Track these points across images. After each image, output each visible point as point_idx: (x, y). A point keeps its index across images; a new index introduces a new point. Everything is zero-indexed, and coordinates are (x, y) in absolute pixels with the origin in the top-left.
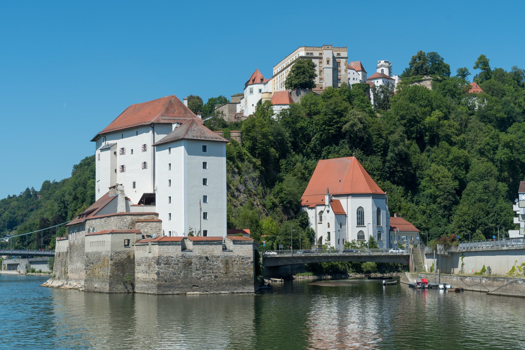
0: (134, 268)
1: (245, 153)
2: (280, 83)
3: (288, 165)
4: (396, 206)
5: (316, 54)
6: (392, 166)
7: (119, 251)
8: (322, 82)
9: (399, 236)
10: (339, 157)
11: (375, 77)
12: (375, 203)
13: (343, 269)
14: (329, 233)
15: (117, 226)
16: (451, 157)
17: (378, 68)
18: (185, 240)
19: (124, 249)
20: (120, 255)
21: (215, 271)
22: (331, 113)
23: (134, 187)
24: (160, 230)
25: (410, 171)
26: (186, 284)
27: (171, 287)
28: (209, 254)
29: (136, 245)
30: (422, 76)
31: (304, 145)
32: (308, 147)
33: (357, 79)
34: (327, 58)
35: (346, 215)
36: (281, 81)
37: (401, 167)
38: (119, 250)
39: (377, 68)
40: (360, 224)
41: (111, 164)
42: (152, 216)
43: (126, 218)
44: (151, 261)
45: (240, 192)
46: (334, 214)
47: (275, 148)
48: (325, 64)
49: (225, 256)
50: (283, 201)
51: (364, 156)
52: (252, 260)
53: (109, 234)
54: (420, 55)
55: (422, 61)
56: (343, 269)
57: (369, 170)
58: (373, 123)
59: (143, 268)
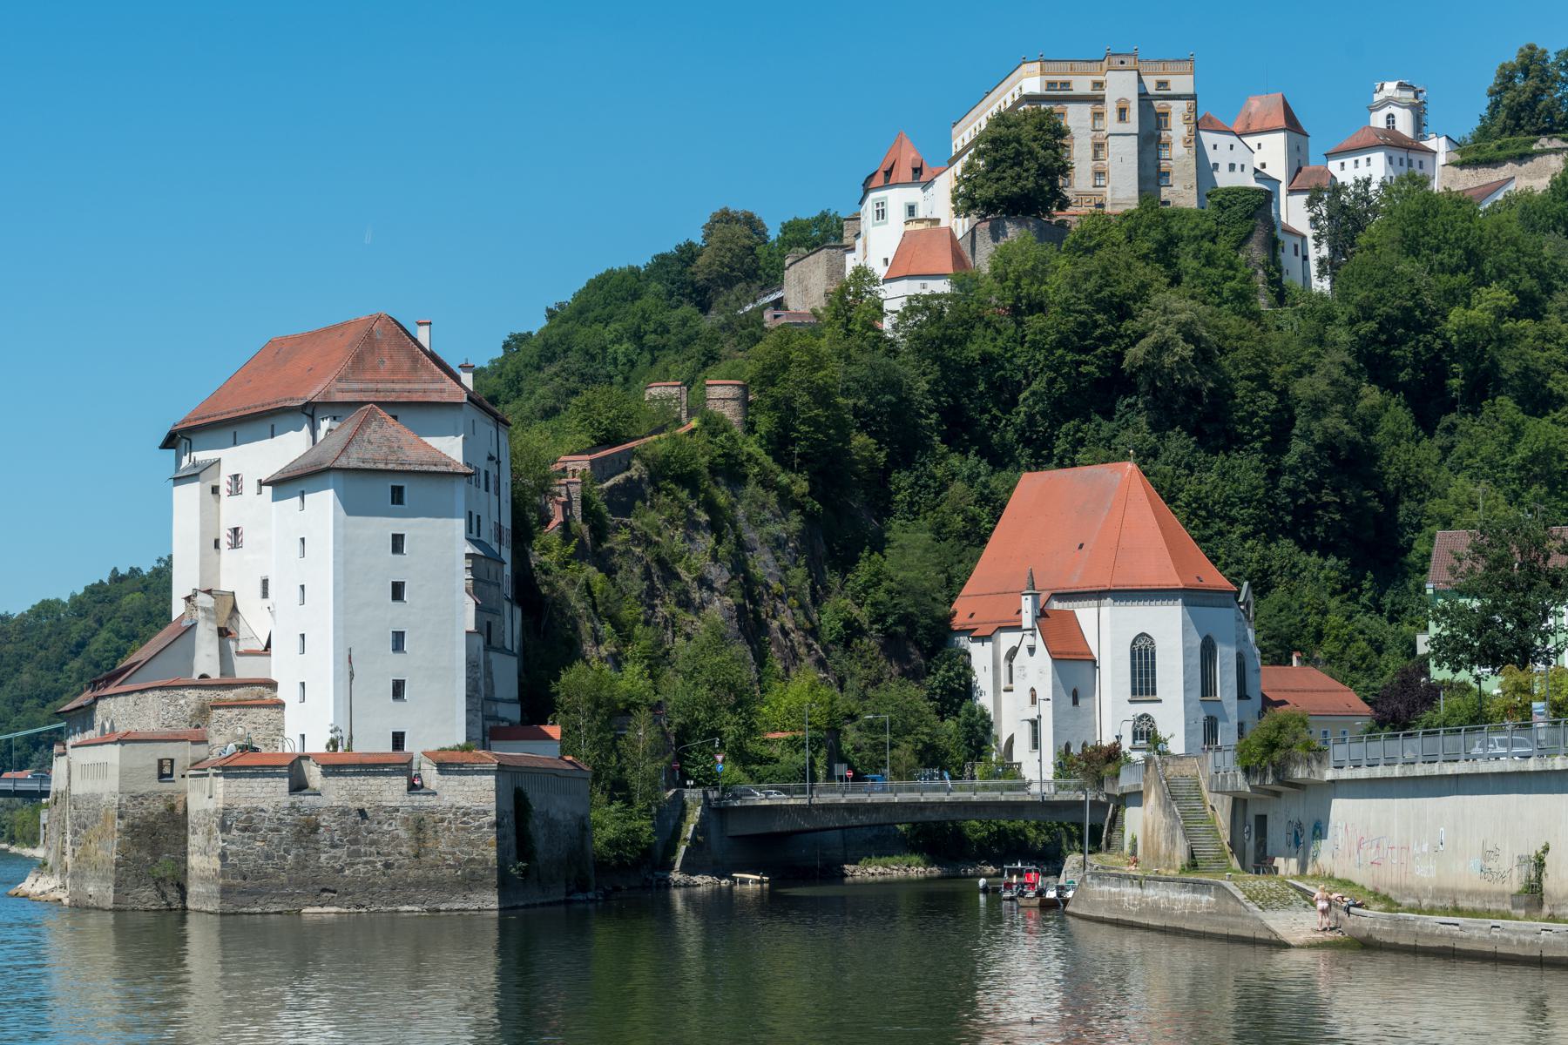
0: (186, 841)
1: (750, 456)
3: (920, 492)
4: (1305, 626)
5: (1082, 85)
6: (1302, 487)
7: (142, 792)
8: (1103, 183)
10: (1107, 460)
11: (1362, 143)
12: (1192, 621)
13: (1044, 844)
14: (1035, 724)
16: (1522, 452)
17: (1374, 108)
18: (304, 763)
19: (156, 786)
20: (146, 803)
22: (1086, 307)
23: (265, 595)
24: (279, 730)
25: (1370, 504)
26: (302, 885)
27: (261, 894)
29: (191, 776)
30: (1532, 137)
31: (995, 417)
32: (1006, 425)
33: (1243, 166)
34: (1117, 98)
35: (1095, 661)
37: (1336, 490)
38: (144, 788)
39: (1372, 111)
40: (1141, 694)
41: (202, 524)
42: (257, 689)
43: (184, 696)
45: (711, 588)
46: (1049, 660)
47: (871, 434)
48: (1111, 122)
49: (414, 808)
50: (885, 615)
51: (1201, 455)
52: (492, 817)
53: (115, 743)
54: (1527, 62)
56: (1044, 844)
57: (1215, 503)
58: (1240, 338)
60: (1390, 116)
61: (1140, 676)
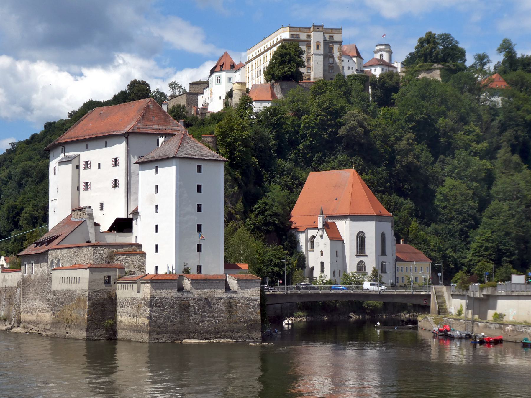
2: (255, 71)
9: (407, 268)
14: (322, 263)
15: (91, 259)
19: (103, 287)
20: (100, 294)
21: (216, 315)
24: (143, 264)
28: (209, 295)
33: (352, 68)
35: (343, 241)
36: (257, 69)
38: (99, 288)
43: (103, 250)
44: (140, 302)
55: (431, 45)
59: (128, 310)
60: (381, 55)
61: (360, 246)
